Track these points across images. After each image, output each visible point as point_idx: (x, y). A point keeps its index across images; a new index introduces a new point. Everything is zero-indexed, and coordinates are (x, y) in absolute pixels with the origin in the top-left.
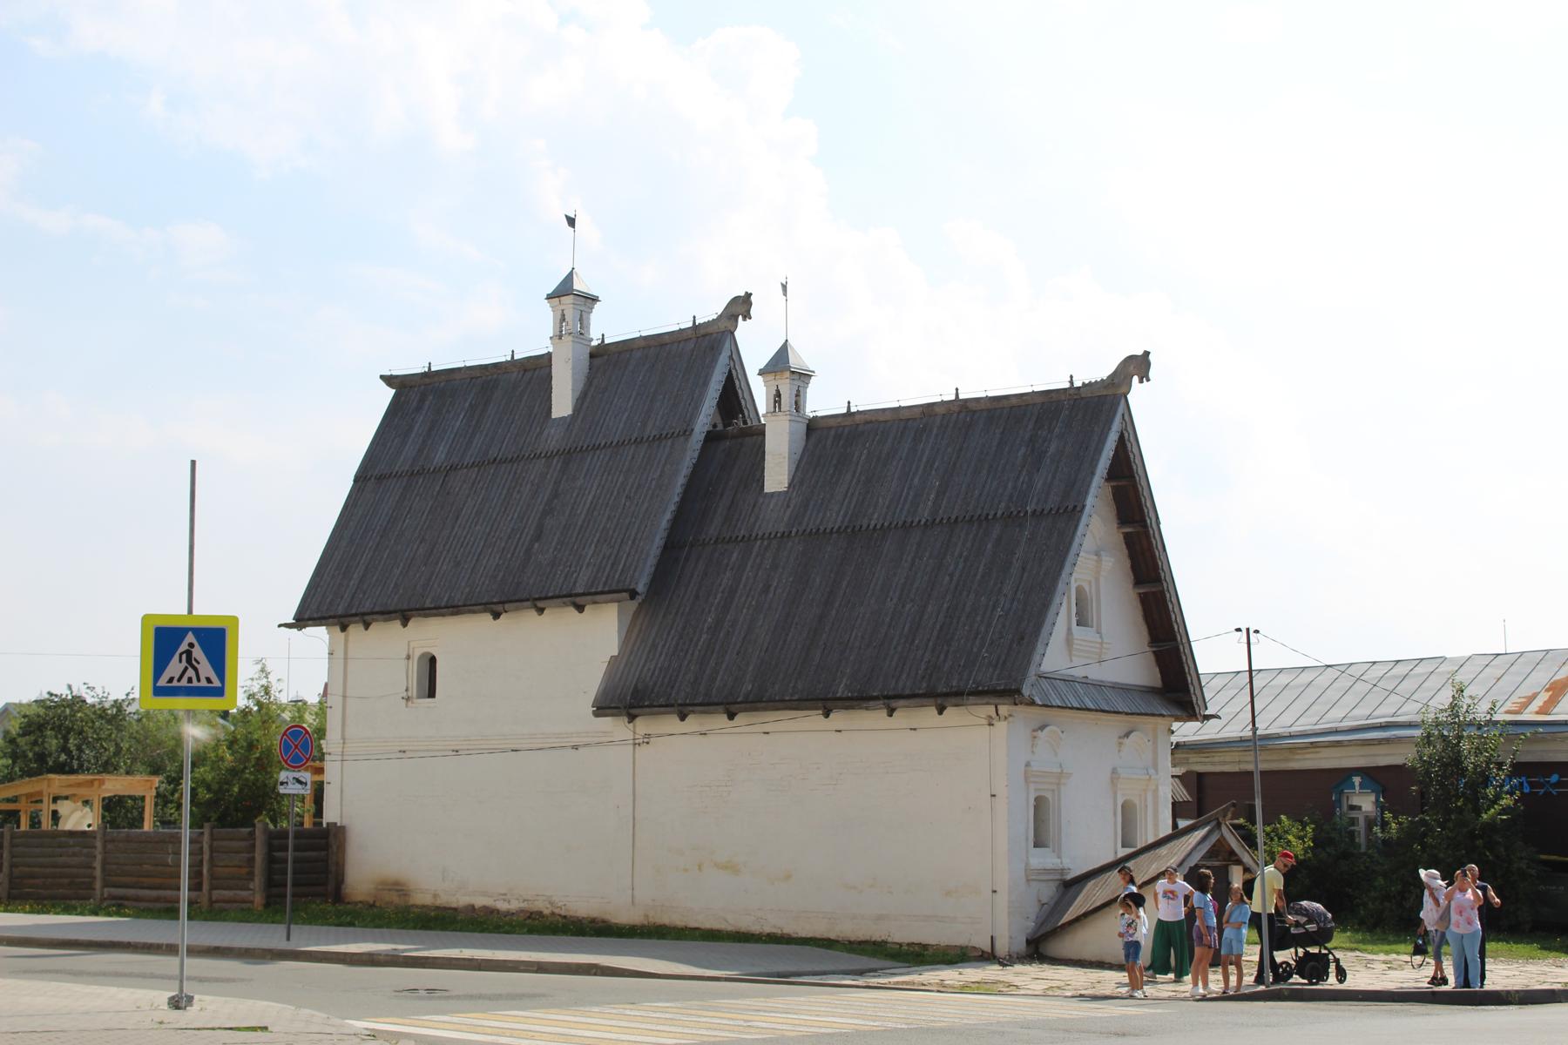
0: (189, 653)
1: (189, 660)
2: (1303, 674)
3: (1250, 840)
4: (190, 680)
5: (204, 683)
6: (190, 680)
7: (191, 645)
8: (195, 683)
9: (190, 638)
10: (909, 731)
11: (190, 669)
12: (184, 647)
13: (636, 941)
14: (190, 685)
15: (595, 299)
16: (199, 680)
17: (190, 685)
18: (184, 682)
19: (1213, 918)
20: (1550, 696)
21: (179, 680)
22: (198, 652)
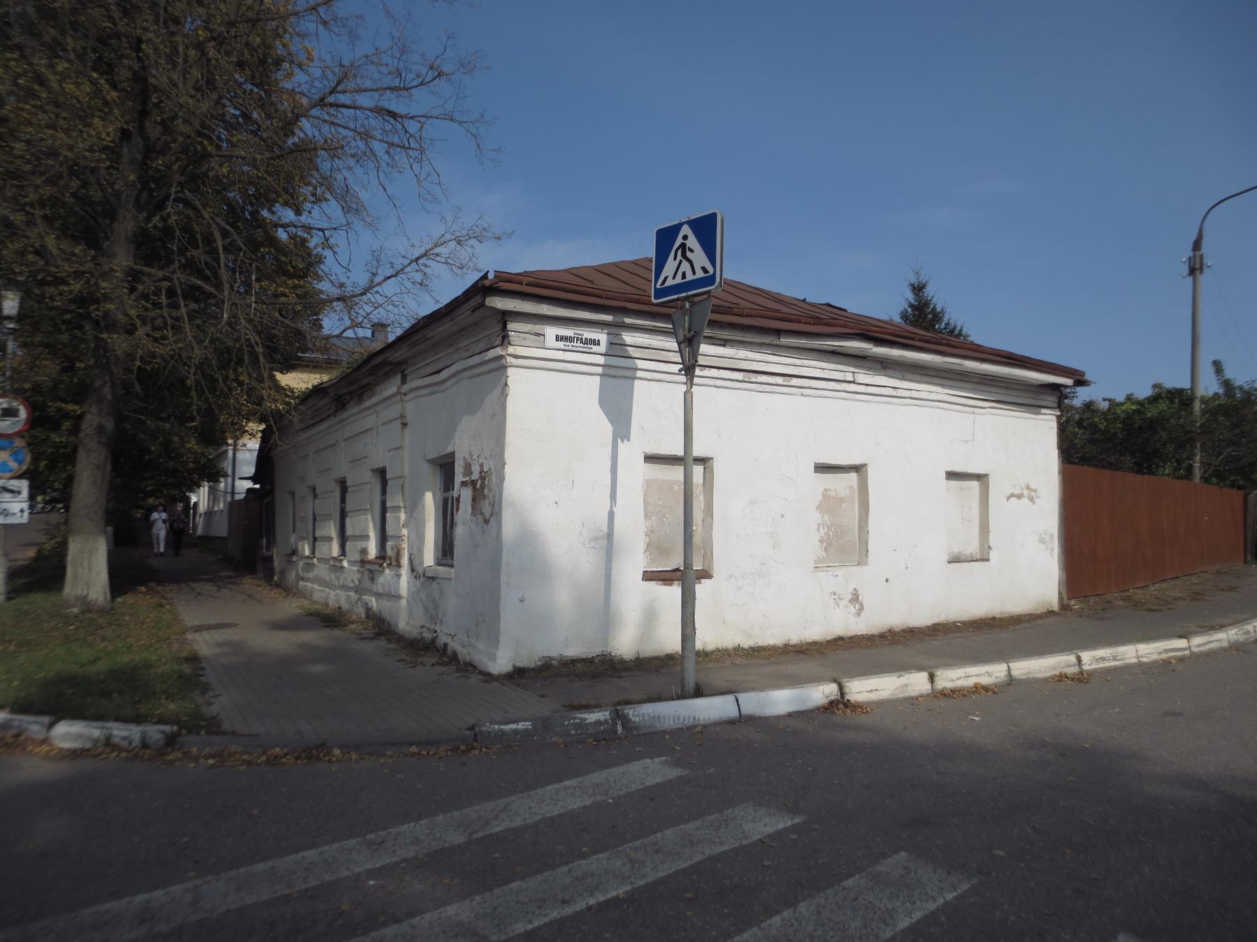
0: (683, 246)
1: (684, 255)
2: (416, 114)
3: (203, 99)
4: (684, 276)
5: (700, 274)
6: (684, 276)
7: (685, 237)
8: (690, 277)
9: (686, 230)
10: (1204, 279)
11: (684, 261)
12: (679, 241)
13: (441, 523)
14: (684, 280)
15: (1008, 500)
16: (694, 273)
17: (684, 280)
18: (679, 280)
19: (307, 586)
20: (670, 784)
21: (674, 278)
22: (692, 242)
